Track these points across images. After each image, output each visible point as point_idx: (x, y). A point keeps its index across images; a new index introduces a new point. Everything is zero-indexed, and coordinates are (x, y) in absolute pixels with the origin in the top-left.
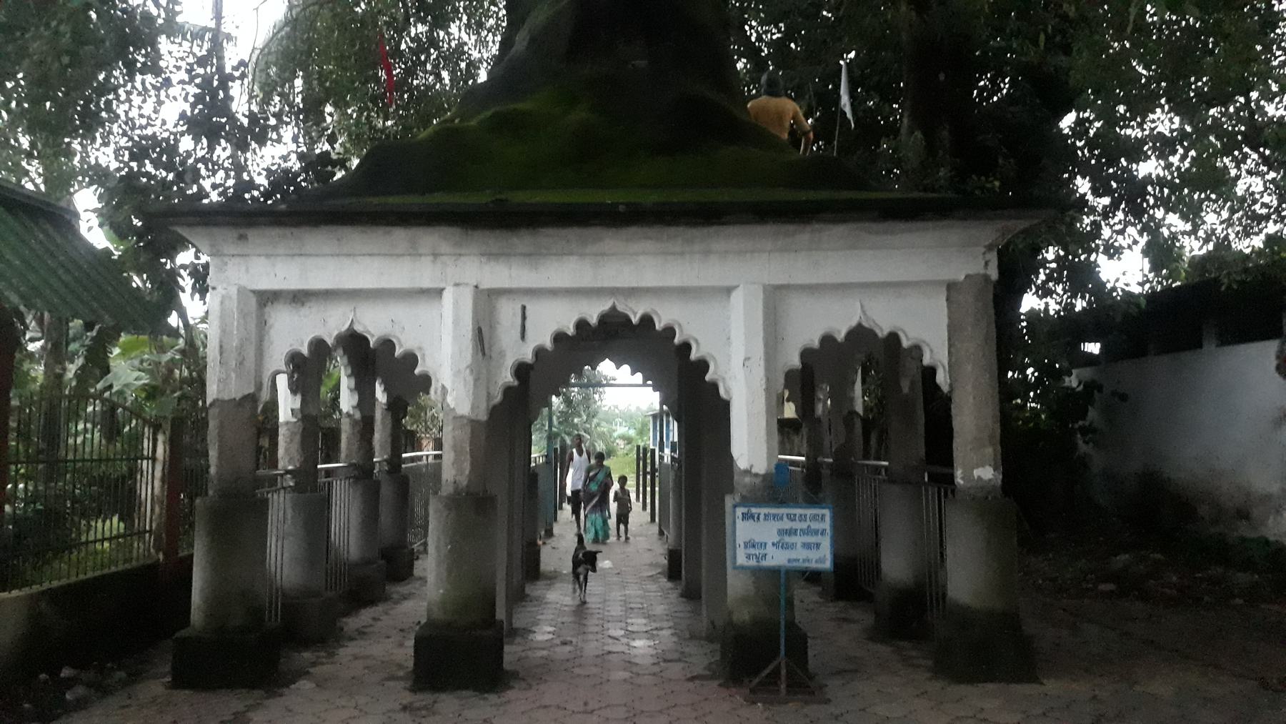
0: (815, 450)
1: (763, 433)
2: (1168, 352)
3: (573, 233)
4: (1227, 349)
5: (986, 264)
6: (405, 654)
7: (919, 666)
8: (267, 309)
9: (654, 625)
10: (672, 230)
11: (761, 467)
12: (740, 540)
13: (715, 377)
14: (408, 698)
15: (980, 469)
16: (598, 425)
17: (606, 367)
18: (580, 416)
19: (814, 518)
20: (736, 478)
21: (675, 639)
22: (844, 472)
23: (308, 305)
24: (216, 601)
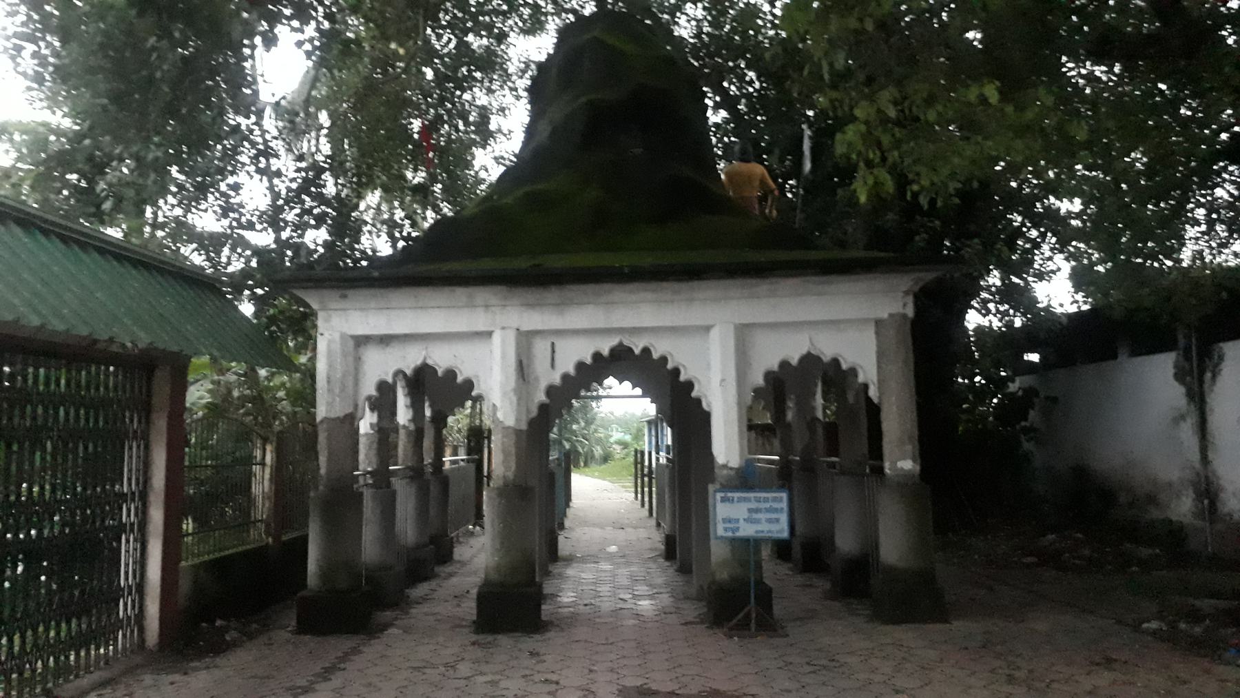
0: (786, 451)
1: (736, 437)
2: (1095, 362)
3: (590, 288)
4: (1140, 359)
5: (905, 305)
6: (469, 609)
7: (859, 615)
8: (362, 350)
9: (655, 591)
10: (665, 284)
11: (735, 462)
12: (719, 517)
13: (699, 394)
14: (474, 638)
15: (902, 462)
16: (596, 431)
17: (610, 381)
18: (578, 423)
19: (775, 500)
20: (716, 470)
21: (672, 599)
22: (809, 467)
23: (393, 344)
24: (326, 573)
